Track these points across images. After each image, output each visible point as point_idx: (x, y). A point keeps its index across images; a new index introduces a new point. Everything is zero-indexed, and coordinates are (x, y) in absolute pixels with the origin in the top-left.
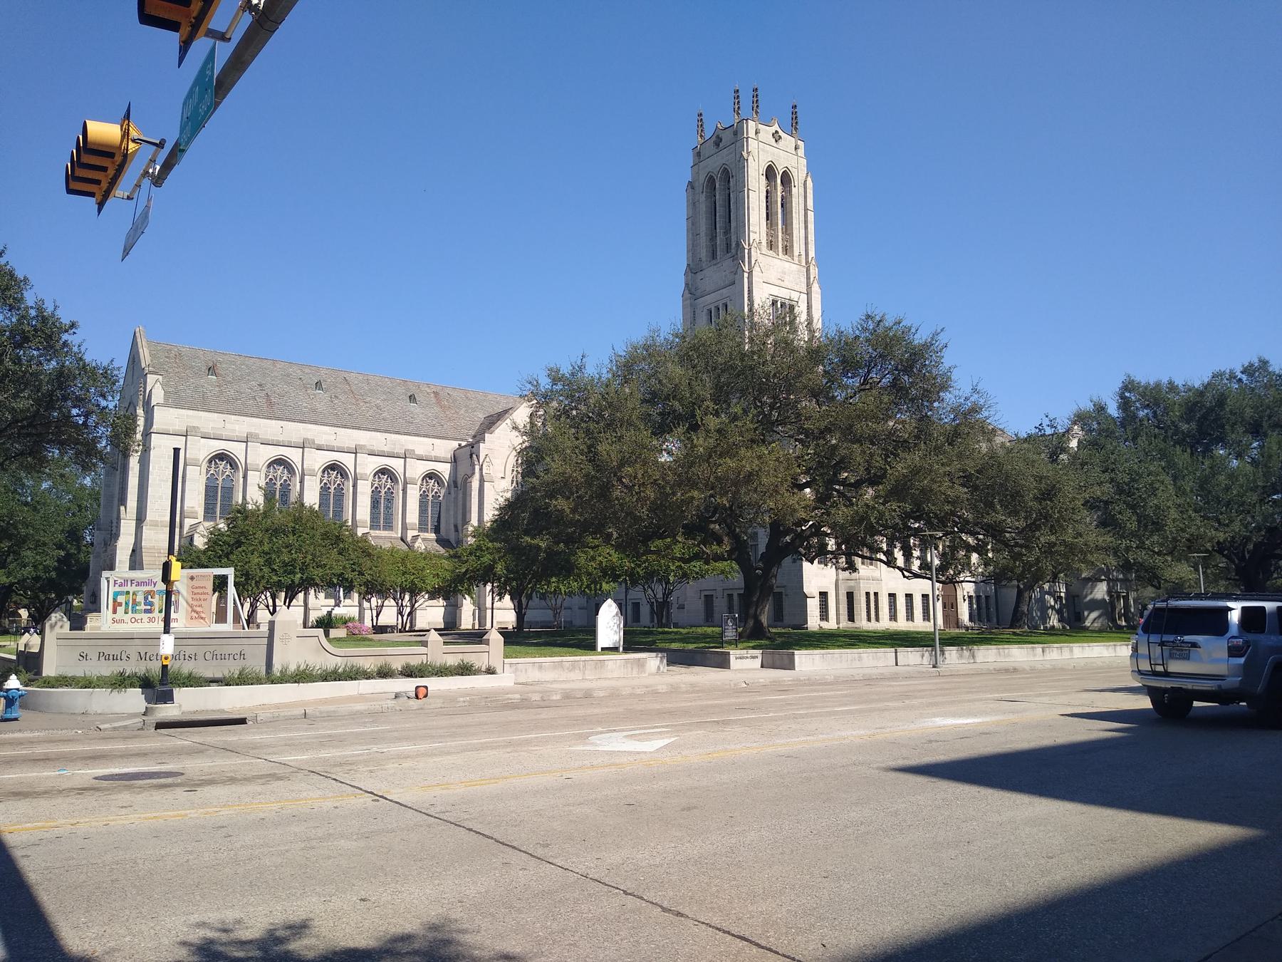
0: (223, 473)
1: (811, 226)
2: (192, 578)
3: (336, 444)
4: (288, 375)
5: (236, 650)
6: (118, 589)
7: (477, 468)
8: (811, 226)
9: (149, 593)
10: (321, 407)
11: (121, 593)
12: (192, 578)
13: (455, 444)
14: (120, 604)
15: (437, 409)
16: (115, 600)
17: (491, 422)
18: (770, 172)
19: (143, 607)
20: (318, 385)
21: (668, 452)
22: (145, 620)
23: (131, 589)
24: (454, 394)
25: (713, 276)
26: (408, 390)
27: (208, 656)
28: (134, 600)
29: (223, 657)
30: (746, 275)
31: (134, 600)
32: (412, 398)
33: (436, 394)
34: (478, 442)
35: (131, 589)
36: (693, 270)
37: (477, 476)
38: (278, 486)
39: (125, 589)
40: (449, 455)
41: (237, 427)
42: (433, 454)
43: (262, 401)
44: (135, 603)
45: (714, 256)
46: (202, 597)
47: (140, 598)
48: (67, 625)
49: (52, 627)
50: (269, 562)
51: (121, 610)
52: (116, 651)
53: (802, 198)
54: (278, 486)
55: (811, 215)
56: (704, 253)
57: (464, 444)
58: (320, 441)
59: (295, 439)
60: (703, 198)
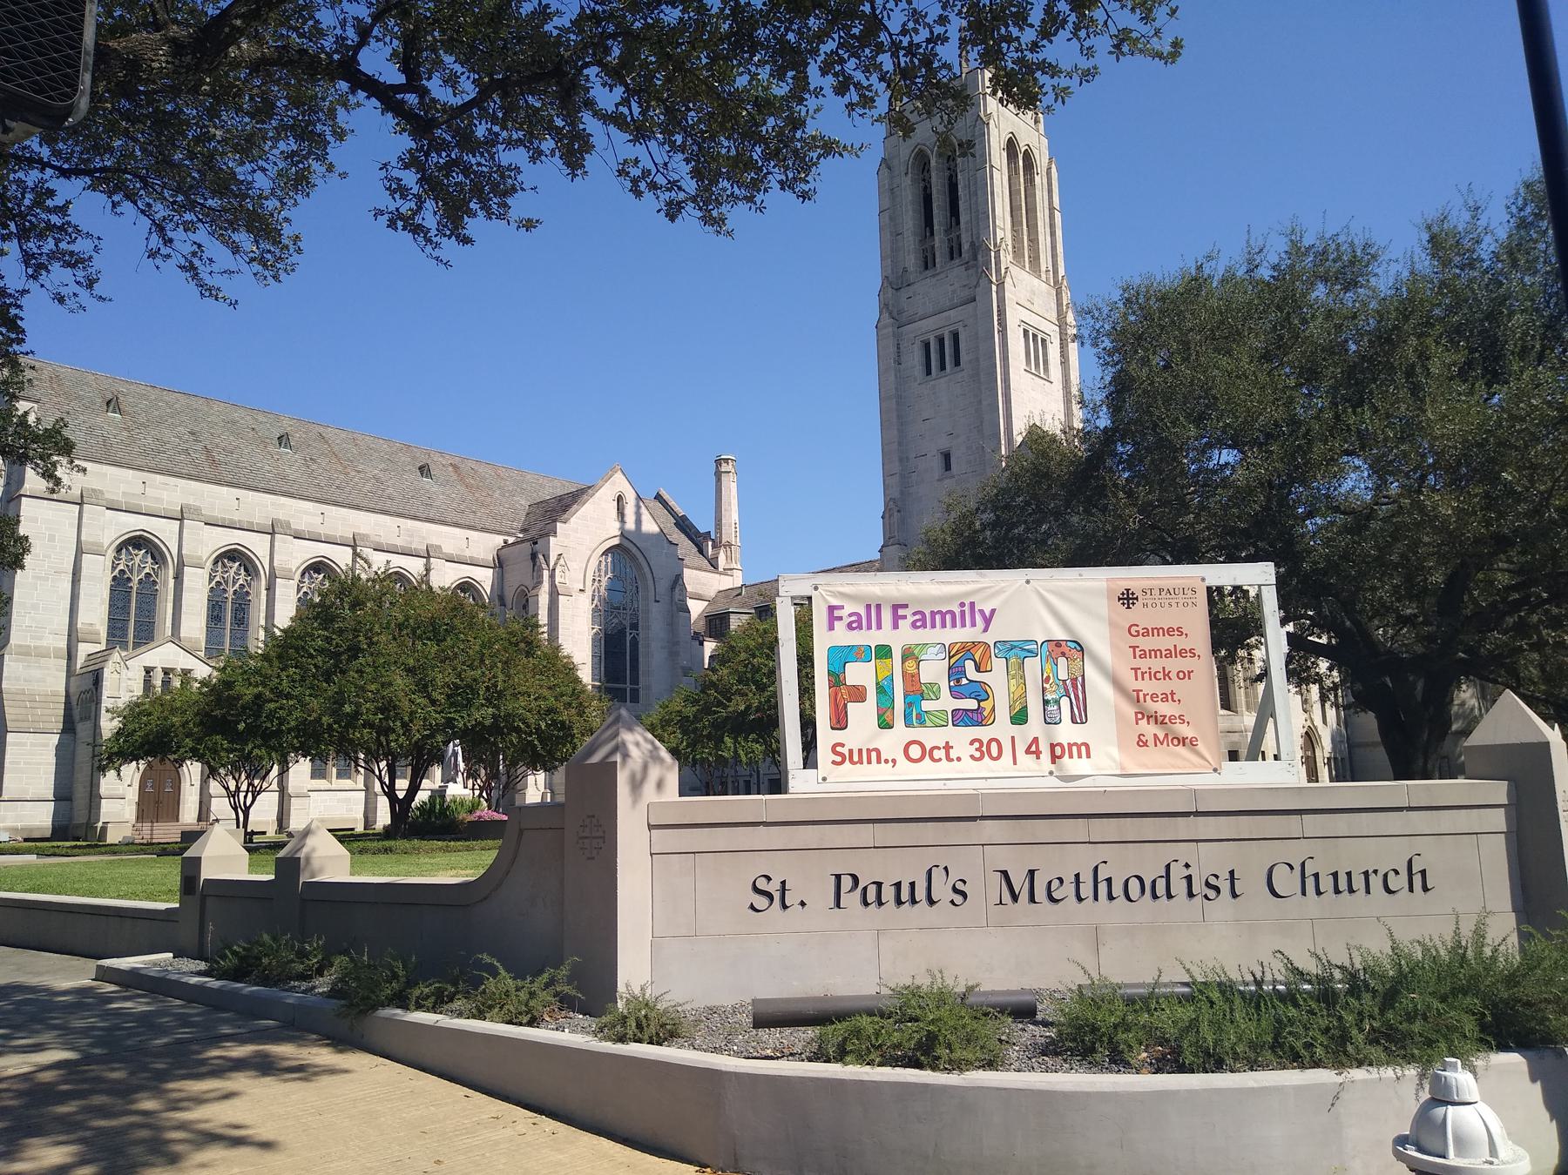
0: (141, 569)
1: (1059, 233)
2: (1128, 598)
3: (323, 531)
4: (234, 422)
5: (1390, 856)
6: (843, 637)
7: (546, 574)
8: (1059, 233)
9: (967, 650)
10: (292, 473)
11: (858, 653)
12: (1128, 598)
13: (499, 540)
14: (859, 694)
15: (462, 489)
16: (836, 680)
17: (560, 507)
18: (1011, 146)
19: (947, 703)
20: (283, 440)
21: (1320, 292)
22: (963, 749)
23: (899, 638)
24: (481, 469)
25: (929, 292)
26: (414, 458)
27: (1286, 881)
28: (911, 680)
29: (1343, 884)
30: (994, 288)
31: (911, 680)
32: (424, 470)
33: (454, 466)
34: (548, 535)
35: (899, 638)
36: (895, 283)
37: (546, 586)
38: (230, 595)
39: (872, 638)
40: (489, 557)
41: (165, 495)
42: (468, 553)
43: (201, 457)
44: (916, 690)
45: (929, 372)
46: (1174, 665)
47: (934, 670)
48: (673, 779)
49: (636, 785)
50: (423, 687)
51: (862, 715)
52: (909, 869)
53: (1047, 191)
54: (230, 595)
55: (1058, 215)
56: (911, 261)
57: (511, 540)
58: (299, 524)
59: (261, 518)
60: (908, 181)
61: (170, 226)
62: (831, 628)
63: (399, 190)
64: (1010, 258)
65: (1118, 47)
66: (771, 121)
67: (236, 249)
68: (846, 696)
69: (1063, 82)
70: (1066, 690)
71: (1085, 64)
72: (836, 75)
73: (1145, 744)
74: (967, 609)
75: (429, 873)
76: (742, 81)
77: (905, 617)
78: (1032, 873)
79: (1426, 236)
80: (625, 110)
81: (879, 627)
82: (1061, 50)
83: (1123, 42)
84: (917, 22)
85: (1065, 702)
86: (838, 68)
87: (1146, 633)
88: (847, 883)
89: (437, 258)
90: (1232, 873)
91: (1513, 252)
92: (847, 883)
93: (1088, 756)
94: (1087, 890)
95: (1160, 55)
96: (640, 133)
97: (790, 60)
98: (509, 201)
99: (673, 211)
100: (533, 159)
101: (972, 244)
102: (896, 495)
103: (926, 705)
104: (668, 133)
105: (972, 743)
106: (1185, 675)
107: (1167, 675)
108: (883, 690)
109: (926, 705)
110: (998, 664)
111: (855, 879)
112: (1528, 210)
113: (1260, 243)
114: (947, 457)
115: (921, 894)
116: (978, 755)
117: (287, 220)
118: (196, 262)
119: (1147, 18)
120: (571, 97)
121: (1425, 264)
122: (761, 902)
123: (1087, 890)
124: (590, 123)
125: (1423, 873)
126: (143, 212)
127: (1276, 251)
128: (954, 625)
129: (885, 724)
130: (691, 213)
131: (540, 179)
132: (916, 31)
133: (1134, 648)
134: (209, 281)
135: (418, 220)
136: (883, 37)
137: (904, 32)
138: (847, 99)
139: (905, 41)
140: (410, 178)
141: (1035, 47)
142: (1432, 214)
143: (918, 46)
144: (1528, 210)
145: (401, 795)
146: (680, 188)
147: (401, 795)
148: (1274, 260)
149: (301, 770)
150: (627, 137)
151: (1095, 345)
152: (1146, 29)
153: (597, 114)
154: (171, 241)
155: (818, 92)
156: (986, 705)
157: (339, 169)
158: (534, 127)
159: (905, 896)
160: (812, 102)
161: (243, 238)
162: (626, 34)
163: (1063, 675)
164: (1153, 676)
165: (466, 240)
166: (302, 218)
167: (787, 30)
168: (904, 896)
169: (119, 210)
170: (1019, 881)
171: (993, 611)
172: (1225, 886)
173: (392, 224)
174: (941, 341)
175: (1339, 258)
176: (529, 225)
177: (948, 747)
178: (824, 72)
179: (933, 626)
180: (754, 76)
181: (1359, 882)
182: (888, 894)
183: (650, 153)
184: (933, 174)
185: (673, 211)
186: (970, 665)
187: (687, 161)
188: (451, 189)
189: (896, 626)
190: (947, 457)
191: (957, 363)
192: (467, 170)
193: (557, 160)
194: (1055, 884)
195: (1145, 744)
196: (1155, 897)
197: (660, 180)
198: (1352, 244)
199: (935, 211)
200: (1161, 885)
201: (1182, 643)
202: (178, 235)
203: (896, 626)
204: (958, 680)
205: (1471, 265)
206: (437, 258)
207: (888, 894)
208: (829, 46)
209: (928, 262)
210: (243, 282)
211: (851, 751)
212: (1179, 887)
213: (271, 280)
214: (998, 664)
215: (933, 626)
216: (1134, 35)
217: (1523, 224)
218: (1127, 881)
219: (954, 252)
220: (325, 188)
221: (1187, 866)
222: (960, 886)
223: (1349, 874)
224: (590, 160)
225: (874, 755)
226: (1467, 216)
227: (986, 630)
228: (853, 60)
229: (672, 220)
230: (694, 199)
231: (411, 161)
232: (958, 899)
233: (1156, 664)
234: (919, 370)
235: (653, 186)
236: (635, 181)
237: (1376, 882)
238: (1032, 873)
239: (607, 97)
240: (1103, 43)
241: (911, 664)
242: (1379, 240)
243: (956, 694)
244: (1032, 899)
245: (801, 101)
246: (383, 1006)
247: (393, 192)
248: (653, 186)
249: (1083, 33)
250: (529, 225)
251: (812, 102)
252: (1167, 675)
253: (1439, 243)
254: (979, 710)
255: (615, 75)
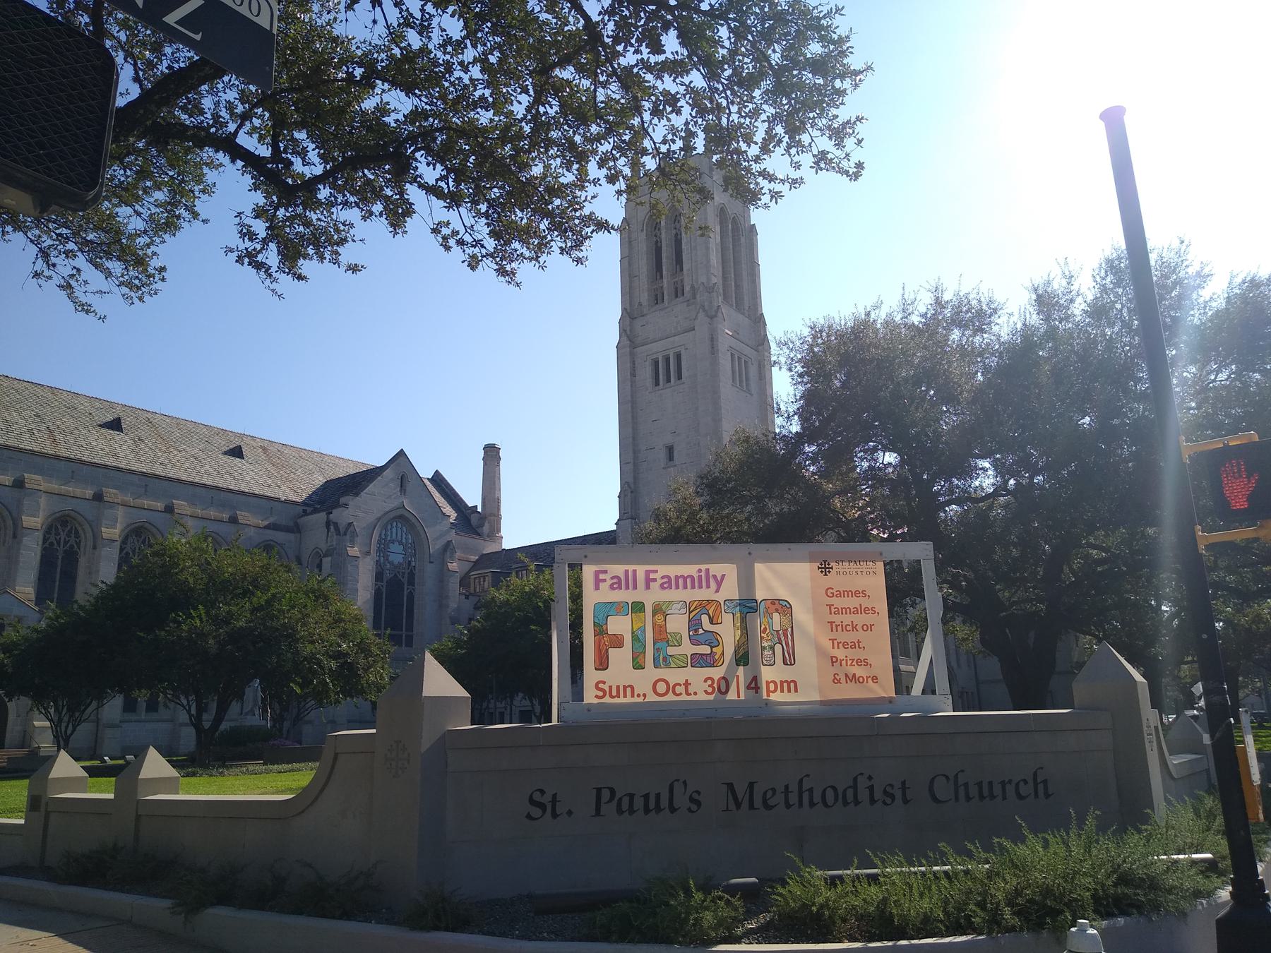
9: (703, 606)
11: (619, 608)
14: (618, 642)
16: (600, 630)
19: (688, 649)
21: (955, 335)
28: (660, 631)
31: (660, 631)
35: (650, 598)
44: (662, 635)
45: (657, 384)
46: (859, 619)
47: (677, 623)
51: (620, 658)
56: (644, 297)
60: (643, 236)
61: (53, 253)
62: (597, 588)
63: (250, 235)
64: (720, 298)
65: (817, 163)
66: (557, 202)
67: (108, 274)
68: (607, 642)
69: (777, 187)
70: (779, 639)
71: (795, 174)
72: (609, 169)
73: (839, 682)
74: (703, 574)
75: (932, 631)
76: (537, 170)
77: (605, 580)
78: (751, 785)
79: (1034, 297)
80: (442, 184)
81: (635, 588)
82: (777, 163)
83: (822, 160)
84: (674, 134)
85: (778, 648)
86: (611, 164)
87: (839, 594)
88: (606, 795)
89: (273, 290)
90: (904, 783)
91: (1098, 311)
92: (606, 795)
93: (796, 691)
94: (793, 798)
95: (846, 173)
96: (454, 200)
97: (579, 157)
98: (340, 250)
99: (473, 263)
100: (364, 218)
101: (692, 287)
102: (631, 480)
103: (671, 651)
104: (475, 203)
105: (705, 681)
106: (870, 627)
107: (854, 628)
108: (638, 639)
109: (671, 651)
110: (727, 618)
111: (612, 791)
112: (1108, 279)
113: (912, 297)
114: (670, 450)
115: (664, 803)
116: (710, 690)
117: (154, 254)
118: (73, 283)
119: (839, 145)
120: (403, 171)
121: (1034, 319)
122: (536, 812)
123: (793, 798)
124: (414, 193)
125: (1045, 782)
126: (32, 241)
127: (924, 303)
128: (693, 587)
129: (638, 665)
130: (488, 267)
131: (367, 232)
132: (674, 141)
133: (830, 606)
134: (83, 299)
135: (260, 258)
136: (647, 144)
137: (664, 142)
138: (617, 187)
139: (664, 149)
140: (260, 227)
141: (757, 159)
142: (1039, 281)
143: (674, 152)
144: (1108, 279)
145: (207, 725)
146: (483, 246)
147: (207, 725)
148: (923, 309)
149: (113, 707)
150: (442, 203)
151: (790, 370)
152: (838, 153)
153: (421, 186)
154: (54, 265)
155: (596, 182)
156: (717, 650)
157: (203, 216)
158: (366, 195)
159: (652, 805)
160: (591, 189)
161: (115, 266)
162: (447, 128)
163: (777, 627)
164: (844, 628)
165: (300, 278)
166: (167, 251)
167: (574, 133)
168: (652, 805)
169: (7, 237)
170: (741, 790)
171: (723, 576)
172: (898, 794)
173: (239, 260)
174: (667, 360)
175: (969, 310)
176: (354, 268)
177: (687, 684)
178: (601, 166)
179: (677, 587)
180: (547, 167)
181: (997, 790)
182: (639, 803)
183: (459, 218)
184: (663, 232)
185: (473, 263)
186: (705, 619)
187: (488, 225)
188: (291, 236)
189: (648, 587)
190: (670, 450)
191: (680, 377)
192: (308, 223)
193: (383, 219)
194: (769, 794)
195: (839, 682)
196: (845, 803)
197: (468, 238)
198: (980, 301)
199: (664, 260)
200: (850, 793)
201: (866, 603)
202: (59, 260)
203: (648, 587)
204: (696, 630)
205: (1067, 319)
206: (273, 290)
207: (639, 803)
208: (606, 147)
209: (657, 299)
210: (112, 301)
211: (610, 687)
212: (864, 795)
213: (136, 300)
214: (727, 618)
215: (677, 587)
216: (830, 156)
217: (1104, 289)
218: (824, 791)
219: (678, 292)
220: (189, 231)
221: (870, 778)
222: (695, 796)
223: (990, 783)
224: (410, 223)
225: (629, 690)
226: (1064, 283)
227: (717, 591)
228: (623, 158)
229: (473, 268)
230: (492, 255)
231: (259, 213)
232: (694, 807)
233: (847, 619)
234: (649, 382)
235: (461, 243)
236: (445, 238)
237: (1010, 789)
238: (751, 785)
239: (430, 173)
240: (807, 159)
241: (659, 618)
242: (999, 298)
243: (694, 642)
244: (751, 806)
245: (582, 188)
246: (213, 905)
247: (243, 235)
248: (461, 243)
249: (793, 151)
250: (354, 268)
251: (591, 189)
252: (854, 628)
253: (1045, 301)
254: (712, 654)
255: (438, 156)
